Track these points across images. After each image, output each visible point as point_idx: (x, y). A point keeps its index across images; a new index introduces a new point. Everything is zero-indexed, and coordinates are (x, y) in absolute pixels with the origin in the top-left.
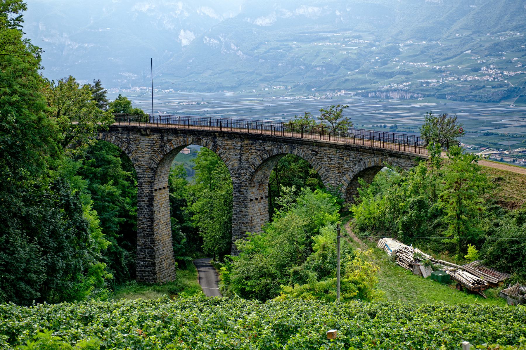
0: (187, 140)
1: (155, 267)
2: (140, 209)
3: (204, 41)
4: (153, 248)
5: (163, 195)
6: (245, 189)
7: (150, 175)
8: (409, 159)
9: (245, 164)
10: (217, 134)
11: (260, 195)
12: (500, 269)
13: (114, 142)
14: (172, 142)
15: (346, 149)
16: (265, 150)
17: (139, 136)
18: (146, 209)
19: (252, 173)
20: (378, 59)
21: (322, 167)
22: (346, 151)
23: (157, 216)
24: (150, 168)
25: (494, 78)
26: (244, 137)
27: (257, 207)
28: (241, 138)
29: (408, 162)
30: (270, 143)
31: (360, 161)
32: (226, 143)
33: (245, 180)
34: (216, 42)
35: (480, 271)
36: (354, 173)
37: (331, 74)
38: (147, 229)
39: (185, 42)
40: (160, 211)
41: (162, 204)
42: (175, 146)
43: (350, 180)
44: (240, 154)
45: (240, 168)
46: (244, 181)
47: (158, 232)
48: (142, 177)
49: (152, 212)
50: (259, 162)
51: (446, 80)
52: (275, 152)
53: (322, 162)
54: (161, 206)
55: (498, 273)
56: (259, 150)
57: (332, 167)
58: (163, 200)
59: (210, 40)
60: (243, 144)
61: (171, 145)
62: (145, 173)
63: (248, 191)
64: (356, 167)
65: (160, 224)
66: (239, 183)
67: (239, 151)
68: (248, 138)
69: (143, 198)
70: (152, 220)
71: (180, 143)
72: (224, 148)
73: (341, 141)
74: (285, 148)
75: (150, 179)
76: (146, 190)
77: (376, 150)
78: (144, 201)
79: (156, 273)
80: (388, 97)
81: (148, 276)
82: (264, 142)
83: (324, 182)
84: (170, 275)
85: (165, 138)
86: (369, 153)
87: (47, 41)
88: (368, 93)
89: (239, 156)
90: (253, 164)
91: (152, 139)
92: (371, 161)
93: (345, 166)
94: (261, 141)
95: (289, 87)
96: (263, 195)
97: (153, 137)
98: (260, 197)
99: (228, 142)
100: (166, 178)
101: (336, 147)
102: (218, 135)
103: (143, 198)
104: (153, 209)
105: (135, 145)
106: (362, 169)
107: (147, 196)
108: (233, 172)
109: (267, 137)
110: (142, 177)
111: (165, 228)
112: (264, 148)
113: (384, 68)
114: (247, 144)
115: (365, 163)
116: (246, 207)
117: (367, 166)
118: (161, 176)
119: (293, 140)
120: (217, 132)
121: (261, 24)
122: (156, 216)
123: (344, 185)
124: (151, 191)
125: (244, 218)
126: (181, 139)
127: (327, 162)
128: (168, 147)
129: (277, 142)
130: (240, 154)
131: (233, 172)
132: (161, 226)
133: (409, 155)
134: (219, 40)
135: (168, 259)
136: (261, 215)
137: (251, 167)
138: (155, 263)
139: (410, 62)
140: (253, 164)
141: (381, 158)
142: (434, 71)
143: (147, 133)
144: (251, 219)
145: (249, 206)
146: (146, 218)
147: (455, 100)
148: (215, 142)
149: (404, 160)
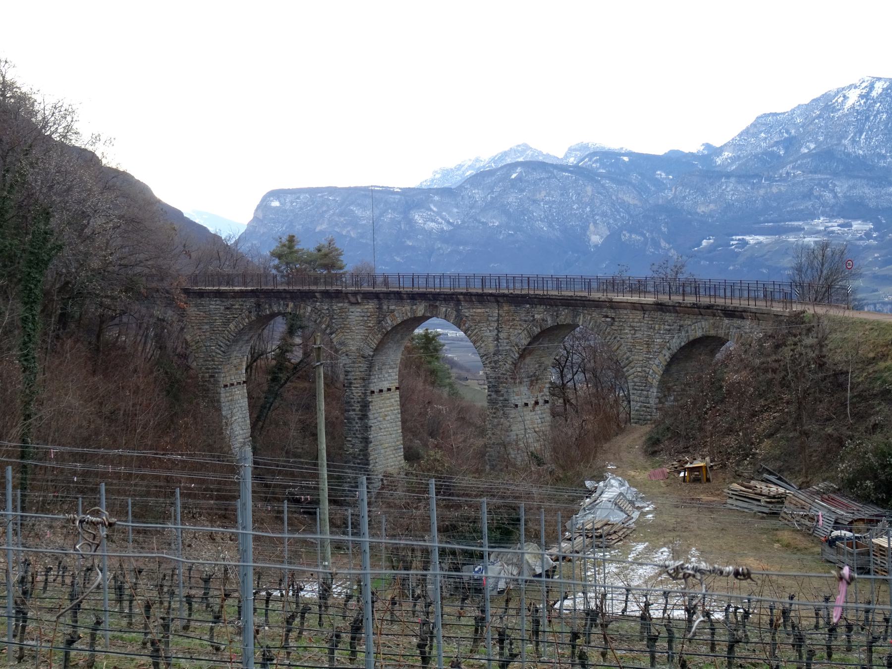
0: (417, 309)
2: (349, 423)
3: (623, 237)
5: (387, 402)
6: (505, 387)
7: (363, 367)
9: (504, 346)
10: (461, 297)
11: (534, 399)
12: (865, 499)
13: (310, 316)
15: (662, 310)
16: (534, 320)
17: (346, 305)
18: (357, 423)
19: (515, 360)
20: (877, 257)
21: (621, 344)
22: (659, 313)
23: (375, 435)
26: (502, 301)
28: (498, 302)
30: (541, 308)
31: (679, 330)
32: (475, 312)
33: (504, 372)
34: (638, 238)
35: (823, 501)
36: (671, 351)
38: (359, 455)
39: (595, 239)
40: (381, 427)
41: (386, 416)
42: (399, 320)
43: (666, 363)
44: (496, 329)
46: (502, 374)
47: (377, 460)
48: (351, 372)
49: (367, 428)
52: (549, 322)
53: (622, 336)
54: (384, 419)
55: (856, 506)
56: (525, 321)
57: (637, 343)
58: (388, 409)
59: (630, 237)
62: (356, 365)
64: (674, 340)
65: (380, 447)
66: (495, 378)
67: (496, 325)
69: (353, 406)
70: (366, 441)
71: (407, 314)
72: (473, 320)
73: (650, 299)
75: (363, 375)
76: (357, 393)
77: (704, 308)
78: (354, 410)
82: (532, 307)
83: (625, 369)
85: (385, 307)
87: (411, 244)
89: (495, 332)
90: (517, 345)
91: (366, 310)
93: (658, 340)
94: (528, 306)
96: (539, 398)
97: (367, 307)
98: (533, 402)
99: (479, 310)
100: (393, 374)
101: (642, 308)
102: (462, 299)
103: (353, 406)
104: (367, 424)
105: (341, 320)
106: (683, 344)
109: (535, 298)
110: (351, 372)
111: (392, 456)
112: (533, 316)
115: (687, 332)
117: (691, 338)
118: (384, 372)
119: (576, 300)
120: (461, 294)
121: (703, 212)
122: (372, 435)
123: (656, 373)
124: (365, 394)
126: (408, 308)
127: (630, 336)
128: (389, 322)
129: (551, 305)
130: (496, 329)
132: (382, 451)
133: (755, 311)
134: (644, 235)
137: (512, 348)
140: (517, 345)
141: (711, 321)
143: (357, 300)
144: (515, 437)
145: (512, 416)
146: (357, 437)
148: (458, 311)
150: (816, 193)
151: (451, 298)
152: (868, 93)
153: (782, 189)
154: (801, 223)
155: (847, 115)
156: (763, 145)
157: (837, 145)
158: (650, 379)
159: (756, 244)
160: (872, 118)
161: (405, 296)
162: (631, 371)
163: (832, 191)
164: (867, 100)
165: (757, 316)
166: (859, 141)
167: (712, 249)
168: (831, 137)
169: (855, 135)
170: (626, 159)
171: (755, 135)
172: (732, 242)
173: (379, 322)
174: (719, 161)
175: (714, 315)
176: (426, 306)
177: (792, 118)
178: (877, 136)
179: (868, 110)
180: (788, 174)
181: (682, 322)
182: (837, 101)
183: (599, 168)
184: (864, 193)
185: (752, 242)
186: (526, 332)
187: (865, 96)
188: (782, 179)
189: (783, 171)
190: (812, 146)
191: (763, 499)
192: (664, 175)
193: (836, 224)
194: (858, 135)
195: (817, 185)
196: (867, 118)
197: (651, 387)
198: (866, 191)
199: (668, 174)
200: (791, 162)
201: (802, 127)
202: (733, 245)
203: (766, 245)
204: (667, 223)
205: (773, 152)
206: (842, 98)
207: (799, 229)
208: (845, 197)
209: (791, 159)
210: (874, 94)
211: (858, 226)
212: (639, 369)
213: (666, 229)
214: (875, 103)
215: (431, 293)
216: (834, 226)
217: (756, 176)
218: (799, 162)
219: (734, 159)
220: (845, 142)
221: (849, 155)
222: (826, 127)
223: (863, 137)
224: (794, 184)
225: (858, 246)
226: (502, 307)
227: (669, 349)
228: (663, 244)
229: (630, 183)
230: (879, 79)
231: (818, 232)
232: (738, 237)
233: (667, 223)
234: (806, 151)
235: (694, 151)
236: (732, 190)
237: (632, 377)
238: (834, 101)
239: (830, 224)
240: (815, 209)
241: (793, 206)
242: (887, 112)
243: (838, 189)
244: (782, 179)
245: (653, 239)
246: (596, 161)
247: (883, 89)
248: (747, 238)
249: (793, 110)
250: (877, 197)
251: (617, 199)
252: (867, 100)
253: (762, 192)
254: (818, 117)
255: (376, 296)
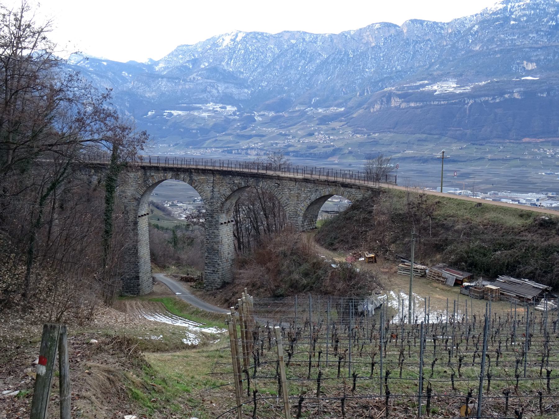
1: (139, 279)
4: (137, 265)
8: (359, 188)
9: (216, 194)
10: (193, 171)
14: (154, 177)
20: (239, 125)
22: (304, 183)
24: (135, 198)
25: (324, 141)
27: (225, 229)
28: (213, 173)
29: (358, 191)
37: (204, 136)
41: (144, 228)
42: (157, 181)
45: (212, 198)
50: (228, 193)
51: (290, 142)
55: (461, 273)
56: (229, 183)
60: (215, 178)
61: (154, 179)
63: (219, 216)
64: (313, 196)
68: (219, 174)
73: (300, 176)
74: (251, 181)
79: (140, 285)
80: (247, 154)
81: (133, 287)
83: (285, 208)
84: (149, 286)
85: (148, 174)
86: (325, 185)
88: (232, 150)
89: (212, 188)
90: (224, 195)
92: (326, 191)
95: (172, 145)
99: (202, 177)
101: (296, 180)
106: (318, 198)
107: (132, 222)
108: (206, 201)
112: (234, 181)
113: (244, 132)
114: (219, 179)
115: (320, 192)
116: (217, 230)
117: (322, 195)
120: (194, 169)
125: (215, 238)
126: (162, 175)
131: (206, 201)
135: (147, 273)
136: (228, 235)
137: (222, 197)
138: (138, 277)
139: (262, 128)
140: (224, 195)
141: (334, 188)
142: (281, 134)
147: (297, 156)
148: (191, 177)
149: (354, 190)
150: (208, 90)
151: (188, 171)
152: (235, 39)
153: (191, 86)
154: (200, 105)
155: (224, 49)
156: (181, 62)
157: (219, 64)
158: (298, 212)
159: (177, 115)
160: (237, 52)
161: (161, 169)
162: (288, 209)
163: (217, 89)
164: (234, 42)
165: (359, 187)
166: (230, 64)
167: (154, 117)
168: (216, 60)
169: (228, 60)
170: (105, 63)
171: (177, 56)
172: (164, 114)
173: (145, 181)
174: (157, 68)
175: (336, 186)
176: (172, 174)
177: (196, 48)
178: (239, 62)
179: (235, 47)
180: (194, 78)
181: (317, 188)
182: (219, 41)
183: (89, 68)
184: (232, 91)
185: (175, 114)
186: (229, 189)
187: (233, 40)
188: (191, 81)
189: (191, 77)
190: (207, 64)
191: (419, 271)
192: (126, 74)
193: (218, 107)
194: (230, 60)
195: (209, 85)
196: (234, 52)
197: (299, 216)
198: (233, 90)
199: (129, 74)
200: (196, 72)
201: (201, 53)
202: (165, 115)
203: (183, 116)
204: (129, 101)
205: (186, 66)
206: (222, 40)
207: (200, 109)
208: (223, 92)
209: (195, 70)
210: (238, 39)
211: (230, 108)
212: (293, 208)
213: (128, 105)
214: (238, 44)
215: (176, 168)
216: (218, 107)
217: (177, 78)
218: (200, 72)
219: (165, 68)
220: (223, 63)
221: (225, 70)
222: (214, 55)
223: (232, 61)
224: (197, 84)
225: (230, 119)
226: (216, 176)
227: (310, 199)
228: (127, 113)
229: (108, 77)
230: (240, 32)
231: (209, 111)
232: (168, 111)
233: (129, 101)
234: (203, 67)
235: (144, 62)
236: (165, 85)
237: (288, 211)
238: (218, 41)
239: (215, 107)
240: (208, 98)
241: (196, 96)
242: (244, 50)
243: (219, 88)
244: (191, 81)
245: (121, 110)
246: (87, 63)
247: (242, 37)
248: (173, 112)
249: (196, 45)
250: (239, 94)
251: (100, 86)
252: (234, 42)
253: (180, 87)
254: (210, 49)
255: (143, 168)
